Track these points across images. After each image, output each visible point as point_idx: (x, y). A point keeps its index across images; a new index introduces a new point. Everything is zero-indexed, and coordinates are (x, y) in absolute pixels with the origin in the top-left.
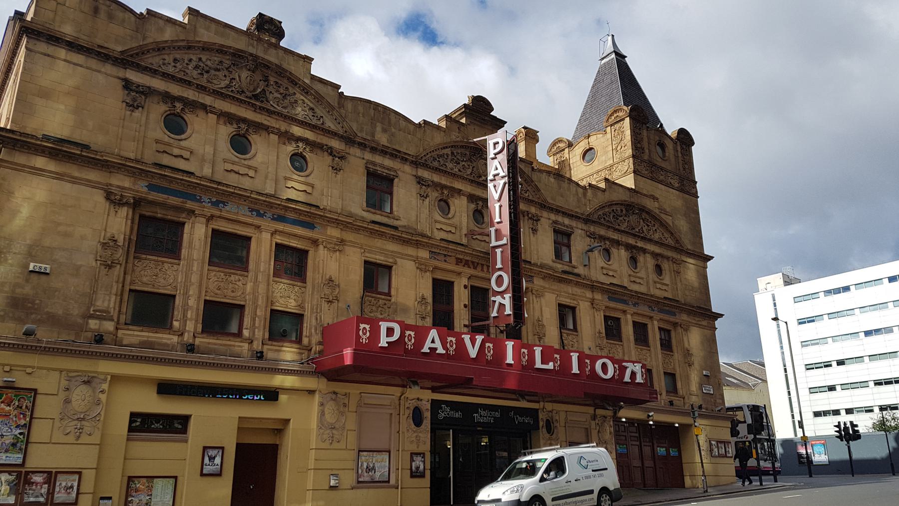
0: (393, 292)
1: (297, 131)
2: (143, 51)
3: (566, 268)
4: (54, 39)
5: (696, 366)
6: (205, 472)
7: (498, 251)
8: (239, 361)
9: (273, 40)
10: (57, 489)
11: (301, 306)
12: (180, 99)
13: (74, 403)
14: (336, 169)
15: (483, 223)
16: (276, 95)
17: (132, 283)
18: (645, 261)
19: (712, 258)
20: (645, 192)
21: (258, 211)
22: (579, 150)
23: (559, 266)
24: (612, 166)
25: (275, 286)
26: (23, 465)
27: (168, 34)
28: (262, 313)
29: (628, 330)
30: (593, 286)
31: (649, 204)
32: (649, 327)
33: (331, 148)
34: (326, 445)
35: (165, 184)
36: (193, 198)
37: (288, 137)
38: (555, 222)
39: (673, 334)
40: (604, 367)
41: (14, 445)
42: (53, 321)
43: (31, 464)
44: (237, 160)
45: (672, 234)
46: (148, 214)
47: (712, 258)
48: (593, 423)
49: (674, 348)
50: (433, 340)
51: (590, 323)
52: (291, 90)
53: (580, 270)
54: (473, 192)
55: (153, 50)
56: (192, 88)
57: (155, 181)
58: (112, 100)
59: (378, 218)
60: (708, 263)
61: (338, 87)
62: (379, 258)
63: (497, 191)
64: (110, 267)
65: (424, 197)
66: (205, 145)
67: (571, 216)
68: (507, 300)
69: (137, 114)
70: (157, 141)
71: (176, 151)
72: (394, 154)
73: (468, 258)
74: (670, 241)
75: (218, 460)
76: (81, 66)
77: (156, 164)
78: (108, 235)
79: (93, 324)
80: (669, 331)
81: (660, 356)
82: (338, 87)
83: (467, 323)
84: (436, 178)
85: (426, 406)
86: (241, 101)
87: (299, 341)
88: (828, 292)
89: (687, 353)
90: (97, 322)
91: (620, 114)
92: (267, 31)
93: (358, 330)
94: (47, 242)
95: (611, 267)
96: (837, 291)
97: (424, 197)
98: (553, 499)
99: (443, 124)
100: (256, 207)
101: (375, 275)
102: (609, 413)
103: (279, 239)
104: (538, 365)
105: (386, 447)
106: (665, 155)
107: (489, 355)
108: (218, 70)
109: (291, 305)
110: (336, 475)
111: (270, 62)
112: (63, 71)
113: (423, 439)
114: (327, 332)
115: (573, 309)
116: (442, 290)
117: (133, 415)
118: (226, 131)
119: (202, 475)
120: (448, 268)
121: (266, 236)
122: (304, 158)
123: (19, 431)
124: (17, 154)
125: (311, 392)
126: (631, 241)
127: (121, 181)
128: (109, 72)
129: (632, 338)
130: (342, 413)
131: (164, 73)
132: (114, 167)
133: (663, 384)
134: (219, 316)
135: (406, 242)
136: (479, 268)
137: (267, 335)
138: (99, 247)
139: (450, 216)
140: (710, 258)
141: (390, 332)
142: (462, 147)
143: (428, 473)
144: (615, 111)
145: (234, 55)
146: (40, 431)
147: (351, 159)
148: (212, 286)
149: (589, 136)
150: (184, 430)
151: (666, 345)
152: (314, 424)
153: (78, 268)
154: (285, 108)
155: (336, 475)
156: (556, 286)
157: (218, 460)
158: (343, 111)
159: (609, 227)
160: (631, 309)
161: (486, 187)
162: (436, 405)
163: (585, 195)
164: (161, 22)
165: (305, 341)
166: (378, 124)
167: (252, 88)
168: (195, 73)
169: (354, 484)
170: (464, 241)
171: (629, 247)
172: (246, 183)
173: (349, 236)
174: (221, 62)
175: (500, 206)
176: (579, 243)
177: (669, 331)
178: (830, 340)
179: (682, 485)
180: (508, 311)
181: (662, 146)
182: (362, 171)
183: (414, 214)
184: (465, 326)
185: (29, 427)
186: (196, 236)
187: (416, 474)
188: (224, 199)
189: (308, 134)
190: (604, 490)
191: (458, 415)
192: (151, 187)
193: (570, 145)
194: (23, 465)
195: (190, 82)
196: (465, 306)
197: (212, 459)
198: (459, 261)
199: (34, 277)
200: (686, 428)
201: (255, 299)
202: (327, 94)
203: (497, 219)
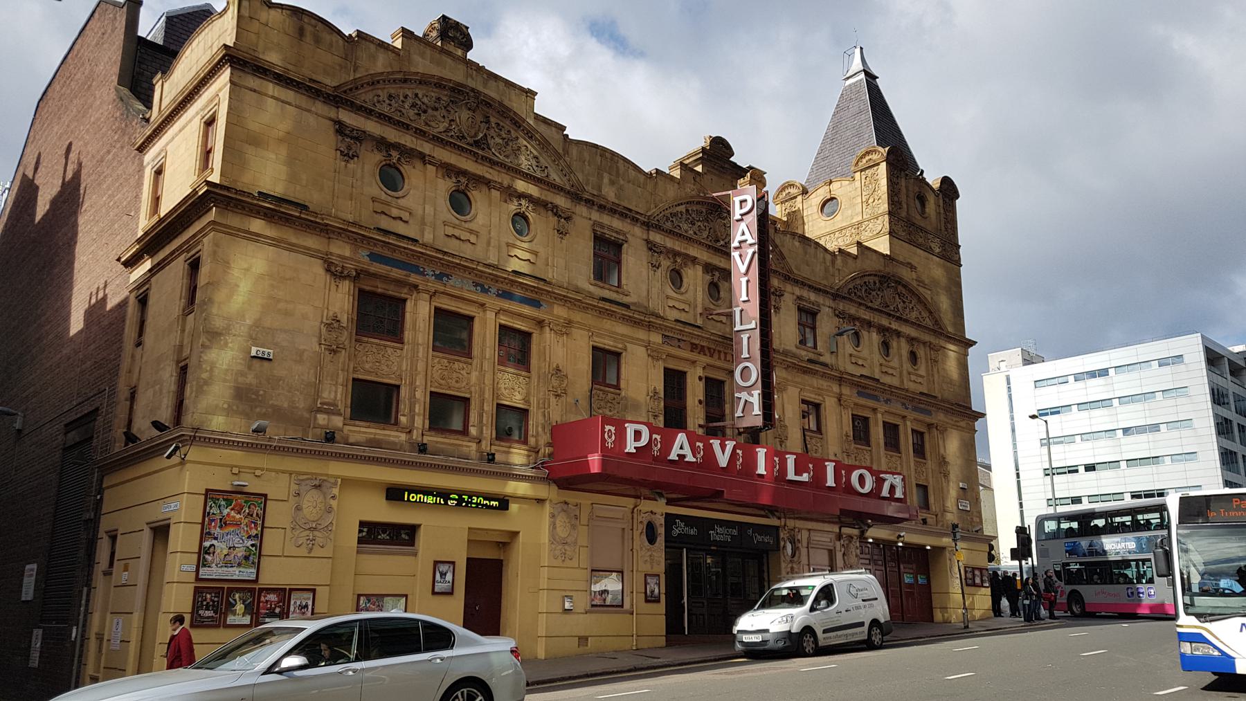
0: (623, 385)
1: (521, 186)
2: (356, 86)
3: (811, 356)
4: (262, 71)
5: (952, 477)
6: (436, 590)
7: (745, 337)
8: (463, 463)
9: (459, 52)
10: (292, 609)
11: (526, 400)
12: (396, 146)
13: (305, 511)
14: (562, 233)
15: (718, 299)
16: (498, 140)
17: (355, 370)
18: (899, 348)
19: (975, 343)
20: (901, 259)
21: (482, 286)
22: (816, 199)
23: (803, 353)
24: (860, 223)
25: (500, 375)
26: (256, 581)
27: (381, 64)
28: (489, 408)
29: (877, 433)
30: (841, 379)
31: (906, 274)
32: (901, 428)
33: (557, 206)
34: (558, 563)
35: (387, 253)
36: (415, 269)
37: (511, 194)
38: (800, 298)
39: (927, 437)
40: (862, 479)
41: (247, 558)
42: (278, 414)
43: (267, 579)
44: (457, 222)
45: (931, 313)
46: (367, 288)
47: (975, 343)
48: (838, 544)
49: (928, 454)
50: (681, 446)
51: (836, 423)
52: (514, 134)
53: (827, 358)
54: (710, 261)
55: (368, 84)
56: (411, 132)
57: (378, 250)
58: (325, 147)
59: (607, 294)
60: (970, 350)
61: (563, 128)
62: (608, 343)
63: (743, 263)
64: (334, 352)
65: (655, 267)
66: (423, 201)
67: (817, 290)
68: (755, 398)
69: (352, 165)
70: (374, 200)
71: (395, 212)
72: (624, 213)
73: (704, 344)
74: (928, 322)
75: (449, 577)
76: (290, 104)
77: (379, 229)
78: (331, 314)
79: (322, 419)
80: (922, 434)
81: (912, 464)
82: (563, 128)
83: (702, 422)
84: (670, 243)
85: (660, 521)
86: (462, 149)
87: (525, 442)
88: (1078, 377)
89: (943, 462)
90: (326, 416)
91: (875, 157)
92: (453, 39)
93: (603, 432)
94: (267, 322)
95: (861, 355)
96: (1093, 374)
97: (655, 267)
98: (825, 631)
99: (677, 174)
100: (481, 281)
101: (605, 361)
102: (855, 532)
103: (504, 320)
104: (791, 475)
105: (619, 567)
106: (924, 209)
107: (656, 450)
108: (436, 109)
109: (516, 400)
110: (571, 597)
111: (492, 99)
112: (275, 111)
113: (654, 559)
114: (558, 432)
115: (817, 406)
116: (675, 380)
117: (362, 524)
118: (445, 186)
119: (434, 593)
120: (681, 357)
121: (490, 315)
122: (526, 218)
123: (251, 543)
124: (230, 214)
125: (540, 501)
126: (885, 322)
127: (341, 249)
128: (320, 112)
129: (882, 442)
130: (574, 527)
131: (380, 114)
132: (333, 232)
133: (915, 498)
134: (445, 409)
135: (636, 323)
136: (716, 356)
137: (427, 426)
138: (324, 330)
139: (683, 290)
140: (971, 343)
141: (638, 435)
142: (698, 203)
143: (663, 598)
144: (868, 153)
145: (453, 90)
146: (272, 543)
147: (576, 219)
148: (436, 376)
149: (831, 182)
150: (411, 542)
151: (919, 451)
152: (545, 538)
153: (301, 353)
154: (507, 157)
155: (571, 597)
156: (800, 378)
157: (449, 577)
158: (567, 159)
159: (860, 304)
160: (882, 407)
161: (728, 255)
162: (670, 519)
163: (833, 262)
164: (372, 47)
165: (532, 441)
166: (606, 175)
167: (473, 132)
168: (412, 113)
169: (588, 608)
170: (699, 322)
171: (882, 330)
172: (467, 251)
173: (577, 316)
174: (439, 99)
175: (748, 281)
176: (826, 324)
177: (922, 434)
178: (1078, 438)
179: (931, 619)
180: (757, 410)
181: (922, 200)
182: (589, 234)
183: (644, 287)
184: (700, 426)
185: (260, 536)
186: (419, 315)
187: (651, 599)
188: (448, 271)
189: (533, 190)
190: (875, 622)
191: (693, 532)
192: (373, 257)
193: (805, 192)
194: (256, 581)
195: (408, 125)
196: (700, 402)
197: (443, 575)
198: (694, 347)
199: (256, 363)
200: (939, 550)
201: (482, 392)
202: (550, 136)
203: (744, 298)
